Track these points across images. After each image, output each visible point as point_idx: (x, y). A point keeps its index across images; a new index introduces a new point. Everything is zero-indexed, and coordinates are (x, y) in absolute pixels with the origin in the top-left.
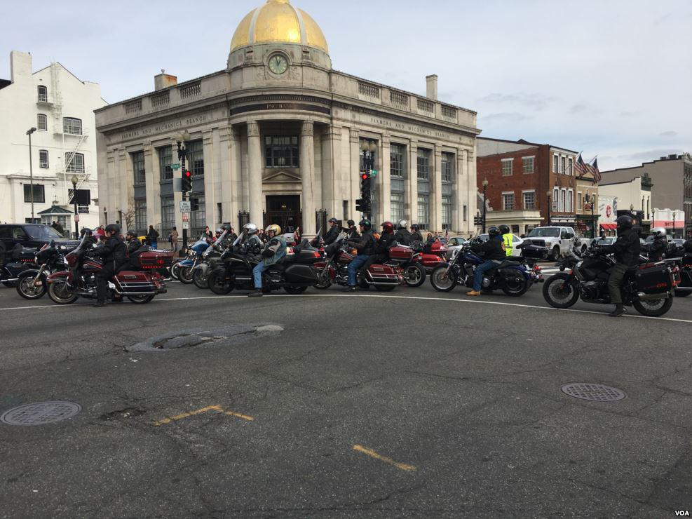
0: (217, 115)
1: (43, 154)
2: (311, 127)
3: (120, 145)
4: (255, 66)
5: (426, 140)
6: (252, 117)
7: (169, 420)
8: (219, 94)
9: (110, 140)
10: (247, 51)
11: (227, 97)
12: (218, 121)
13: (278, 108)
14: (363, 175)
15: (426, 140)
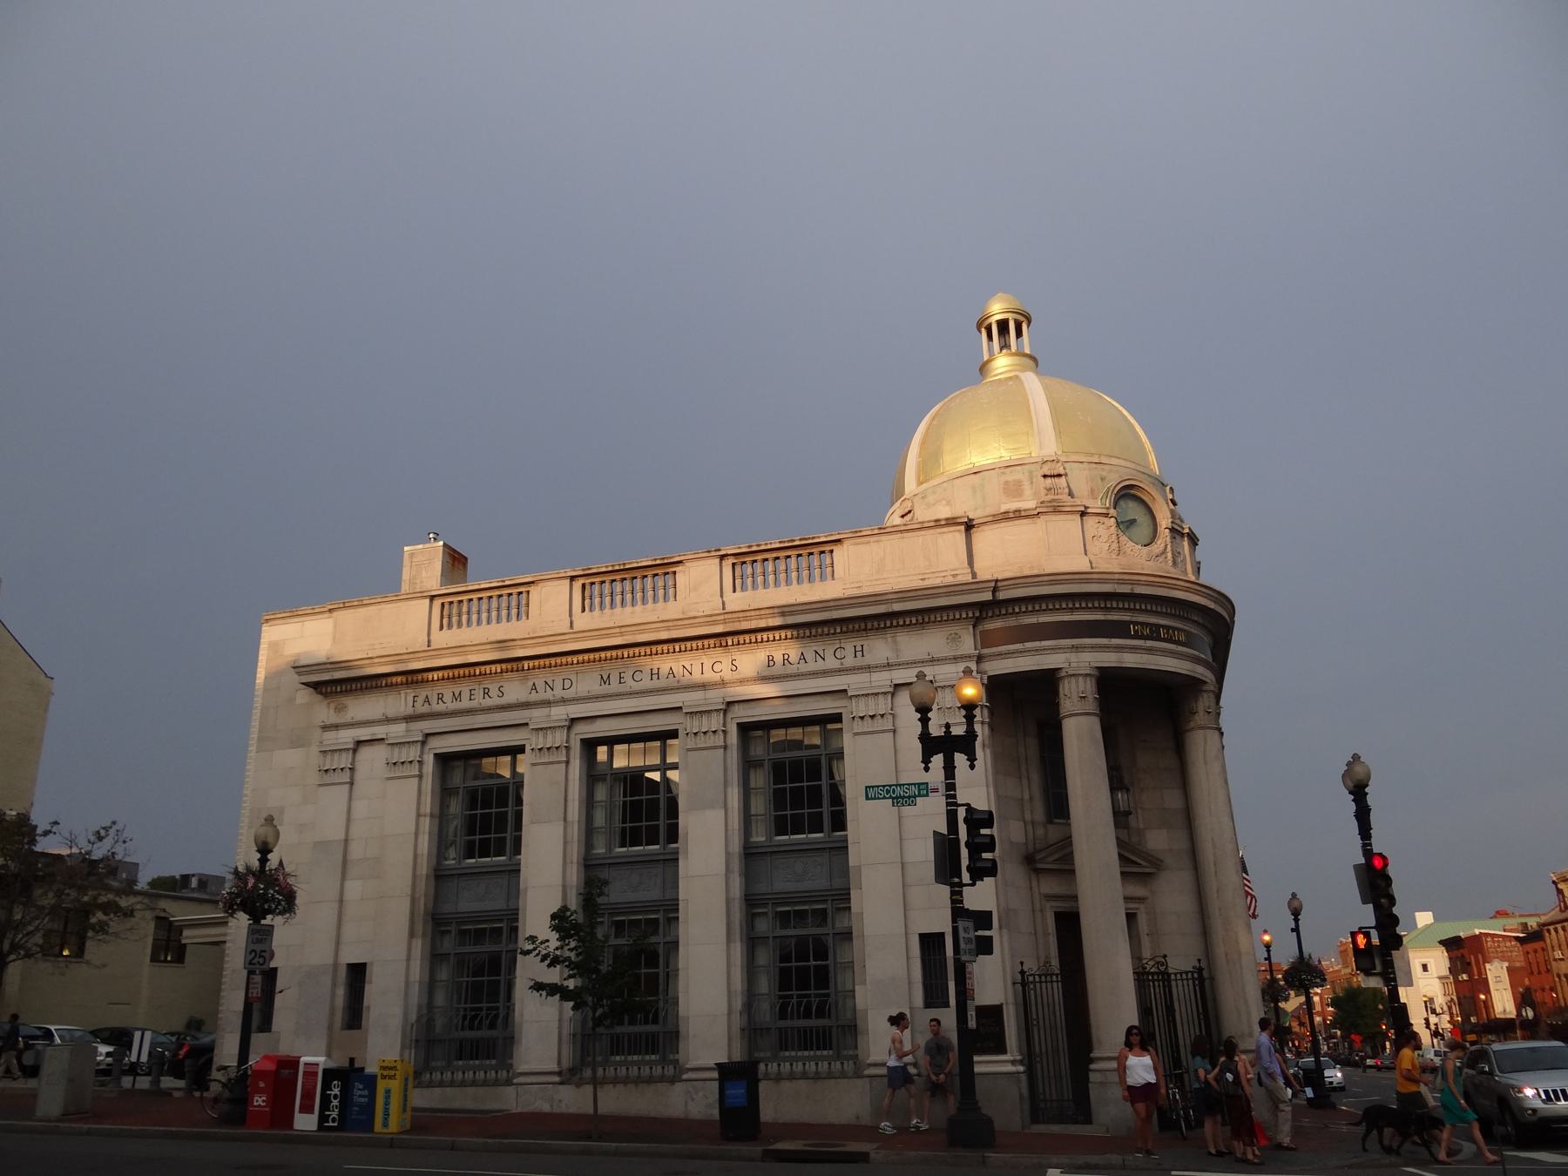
2: (1088, 687)
9: (340, 709)
13: (1158, 639)
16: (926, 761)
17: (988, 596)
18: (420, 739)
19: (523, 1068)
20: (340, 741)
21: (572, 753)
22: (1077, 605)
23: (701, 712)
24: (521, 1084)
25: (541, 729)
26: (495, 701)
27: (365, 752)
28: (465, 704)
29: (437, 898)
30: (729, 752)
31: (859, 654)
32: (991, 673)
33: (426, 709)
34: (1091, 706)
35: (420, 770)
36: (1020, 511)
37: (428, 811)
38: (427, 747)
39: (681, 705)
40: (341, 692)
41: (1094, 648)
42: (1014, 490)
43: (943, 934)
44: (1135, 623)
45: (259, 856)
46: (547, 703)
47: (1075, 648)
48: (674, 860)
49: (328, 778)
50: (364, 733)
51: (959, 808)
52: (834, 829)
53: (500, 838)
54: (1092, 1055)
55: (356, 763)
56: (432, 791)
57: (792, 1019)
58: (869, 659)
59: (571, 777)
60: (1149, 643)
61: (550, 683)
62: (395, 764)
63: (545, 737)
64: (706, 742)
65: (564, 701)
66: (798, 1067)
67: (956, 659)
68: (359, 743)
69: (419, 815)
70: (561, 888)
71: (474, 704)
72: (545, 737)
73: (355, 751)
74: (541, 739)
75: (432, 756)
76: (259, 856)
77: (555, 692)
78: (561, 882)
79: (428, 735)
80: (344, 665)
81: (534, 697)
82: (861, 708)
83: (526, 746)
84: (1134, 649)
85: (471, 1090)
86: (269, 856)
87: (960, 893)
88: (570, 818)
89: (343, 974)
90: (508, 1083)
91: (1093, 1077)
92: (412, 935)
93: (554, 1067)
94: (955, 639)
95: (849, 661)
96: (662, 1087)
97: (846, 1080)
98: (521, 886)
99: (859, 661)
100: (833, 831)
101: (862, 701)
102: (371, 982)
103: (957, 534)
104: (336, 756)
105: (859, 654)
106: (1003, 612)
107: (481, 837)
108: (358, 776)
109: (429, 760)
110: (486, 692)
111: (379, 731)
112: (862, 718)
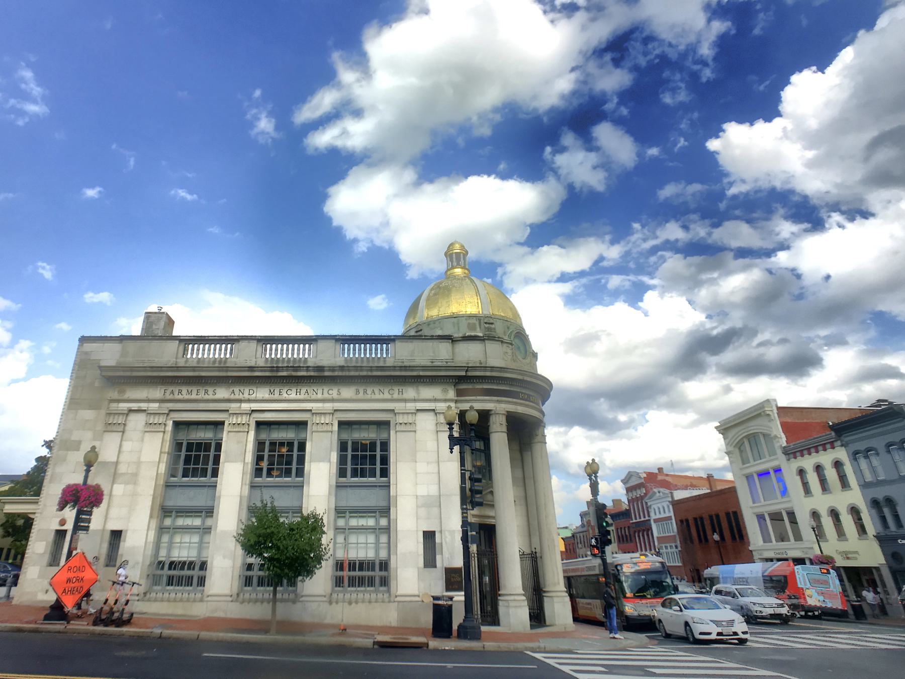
0: (433, 392)
1: (808, 493)
2: (503, 420)
3: (156, 405)
4: (502, 342)
5: (202, 406)
6: (503, 406)
7: (865, 593)
8: (435, 364)
10: (485, 321)
11: (467, 371)
12: (435, 400)
14: (250, 567)
15: (202, 406)
16: (451, 449)
17: (463, 373)
18: (126, 412)
19: (399, 593)
20: (119, 408)
21: (250, 428)
22: (448, 381)
23: (321, 413)
24: (209, 601)
25: (235, 414)
26: (211, 397)
27: (133, 417)
28: (194, 396)
29: (164, 498)
30: (166, 435)
31: (401, 393)
32: (461, 409)
33: (171, 397)
34: (504, 429)
35: (165, 429)
36: (433, 336)
37: (167, 451)
38: (169, 417)
39: (311, 408)
40: (123, 383)
41: (509, 402)
42: (471, 327)
43: (434, 532)
44: (522, 393)
45: (85, 468)
46: (240, 401)
47: (498, 401)
48: (301, 487)
49: (110, 428)
50: (134, 406)
51: (467, 472)
52: (297, 476)
53: (187, 468)
54: (500, 593)
55: (127, 422)
56: (170, 440)
57: (368, 570)
58: (405, 396)
59: (249, 440)
60: (527, 403)
61: (241, 393)
62: (150, 424)
63: (237, 418)
64: (322, 428)
65: (249, 401)
66: (254, 596)
67: (446, 401)
68: (131, 411)
69: (161, 452)
70: (239, 498)
71: (199, 397)
72: (237, 418)
73: (127, 415)
74: (234, 419)
75: (171, 422)
76: (85, 468)
77: (244, 396)
78: (239, 494)
79: (171, 411)
80: (525, 373)
81: (232, 397)
82: (317, 419)
83: (309, 422)
84: (521, 404)
85: (180, 604)
86: (92, 468)
87: (467, 513)
88: (246, 461)
89: (107, 536)
90: (201, 600)
91: (501, 603)
92: (151, 517)
93: (227, 592)
94: (445, 391)
95: (396, 396)
96: (290, 604)
97: (149, 603)
98: (217, 494)
99: (400, 397)
100: (212, 477)
101: (401, 416)
102: (125, 541)
103: (448, 344)
104: (116, 417)
105: (401, 393)
106: (419, 381)
107: (189, 467)
108: (127, 428)
109: (170, 424)
110: (172, 392)
111: (143, 406)
112: (401, 424)
